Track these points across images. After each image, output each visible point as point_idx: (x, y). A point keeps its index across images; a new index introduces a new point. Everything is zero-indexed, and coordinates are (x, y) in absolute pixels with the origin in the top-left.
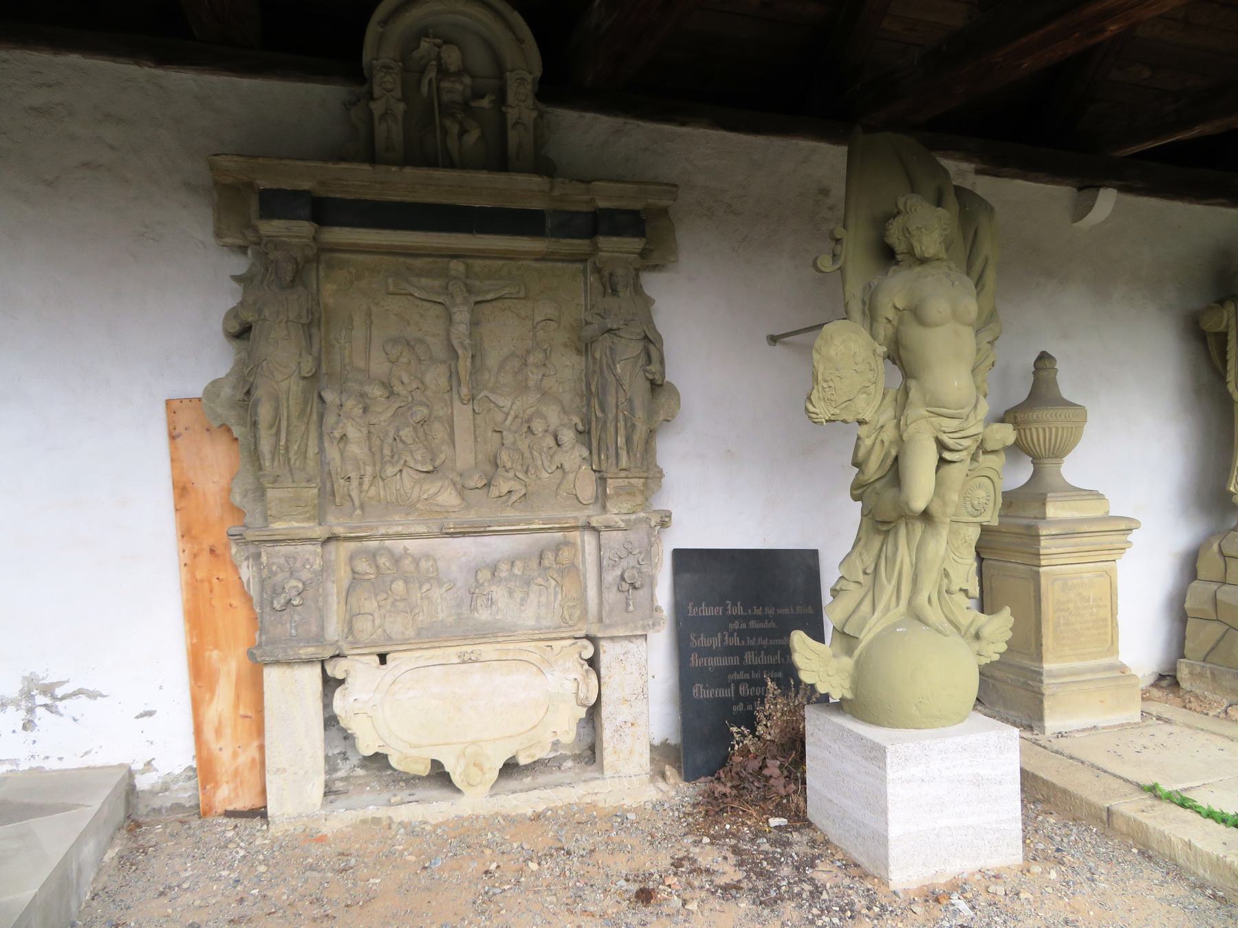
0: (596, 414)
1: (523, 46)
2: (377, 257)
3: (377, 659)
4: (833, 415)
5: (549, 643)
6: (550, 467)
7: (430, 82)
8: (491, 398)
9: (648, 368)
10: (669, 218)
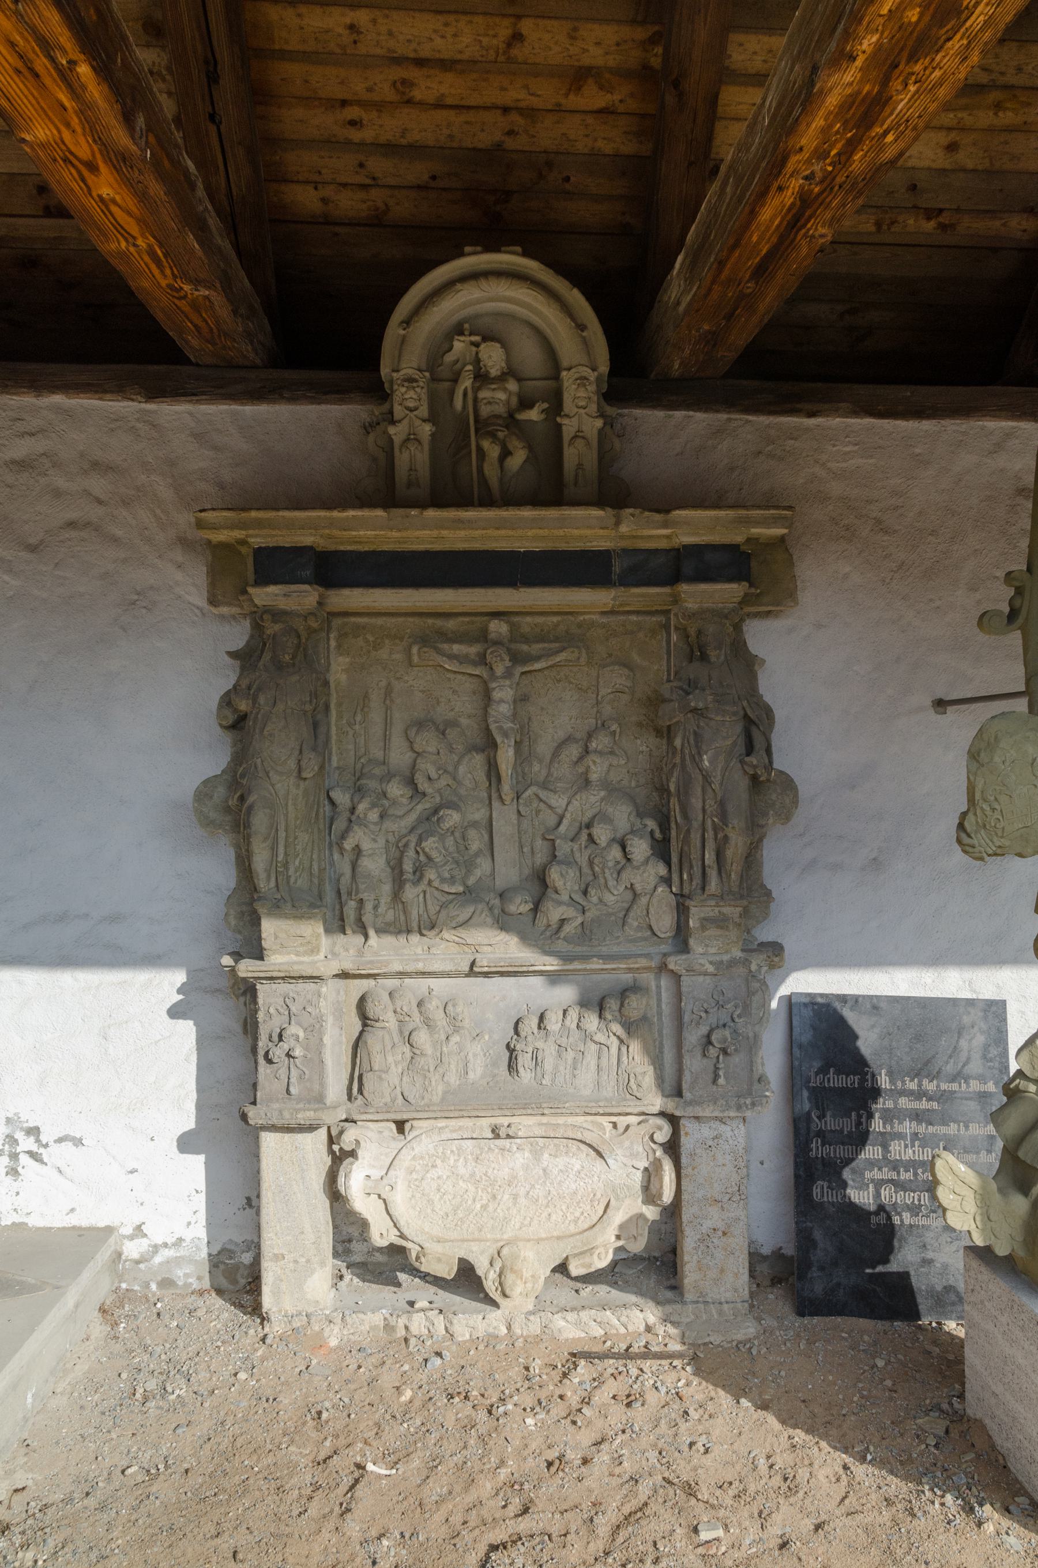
0: (676, 821)
1: (584, 334)
2: (401, 620)
3: (393, 1126)
4: (1000, 847)
5: (614, 1119)
6: (615, 887)
7: (465, 394)
8: (541, 796)
9: (747, 759)
10: (787, 549)
